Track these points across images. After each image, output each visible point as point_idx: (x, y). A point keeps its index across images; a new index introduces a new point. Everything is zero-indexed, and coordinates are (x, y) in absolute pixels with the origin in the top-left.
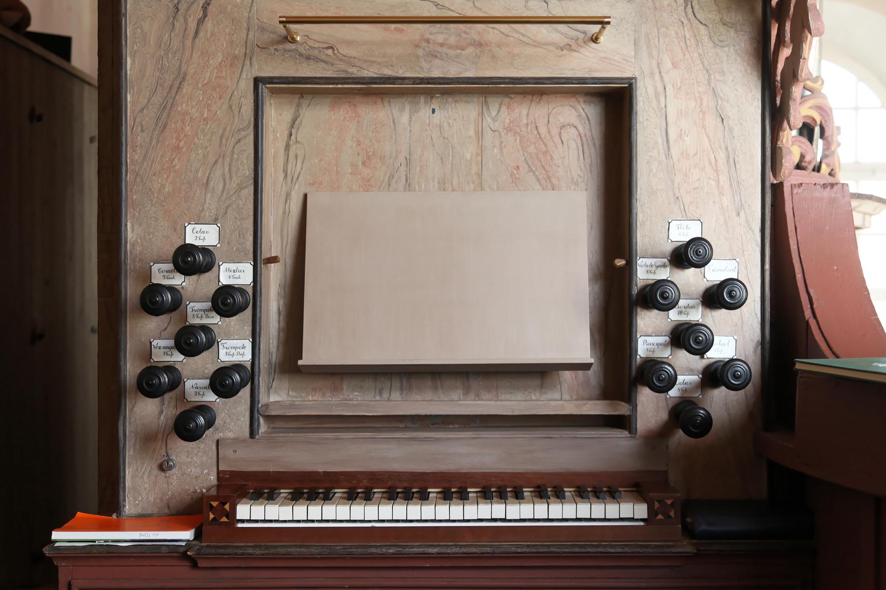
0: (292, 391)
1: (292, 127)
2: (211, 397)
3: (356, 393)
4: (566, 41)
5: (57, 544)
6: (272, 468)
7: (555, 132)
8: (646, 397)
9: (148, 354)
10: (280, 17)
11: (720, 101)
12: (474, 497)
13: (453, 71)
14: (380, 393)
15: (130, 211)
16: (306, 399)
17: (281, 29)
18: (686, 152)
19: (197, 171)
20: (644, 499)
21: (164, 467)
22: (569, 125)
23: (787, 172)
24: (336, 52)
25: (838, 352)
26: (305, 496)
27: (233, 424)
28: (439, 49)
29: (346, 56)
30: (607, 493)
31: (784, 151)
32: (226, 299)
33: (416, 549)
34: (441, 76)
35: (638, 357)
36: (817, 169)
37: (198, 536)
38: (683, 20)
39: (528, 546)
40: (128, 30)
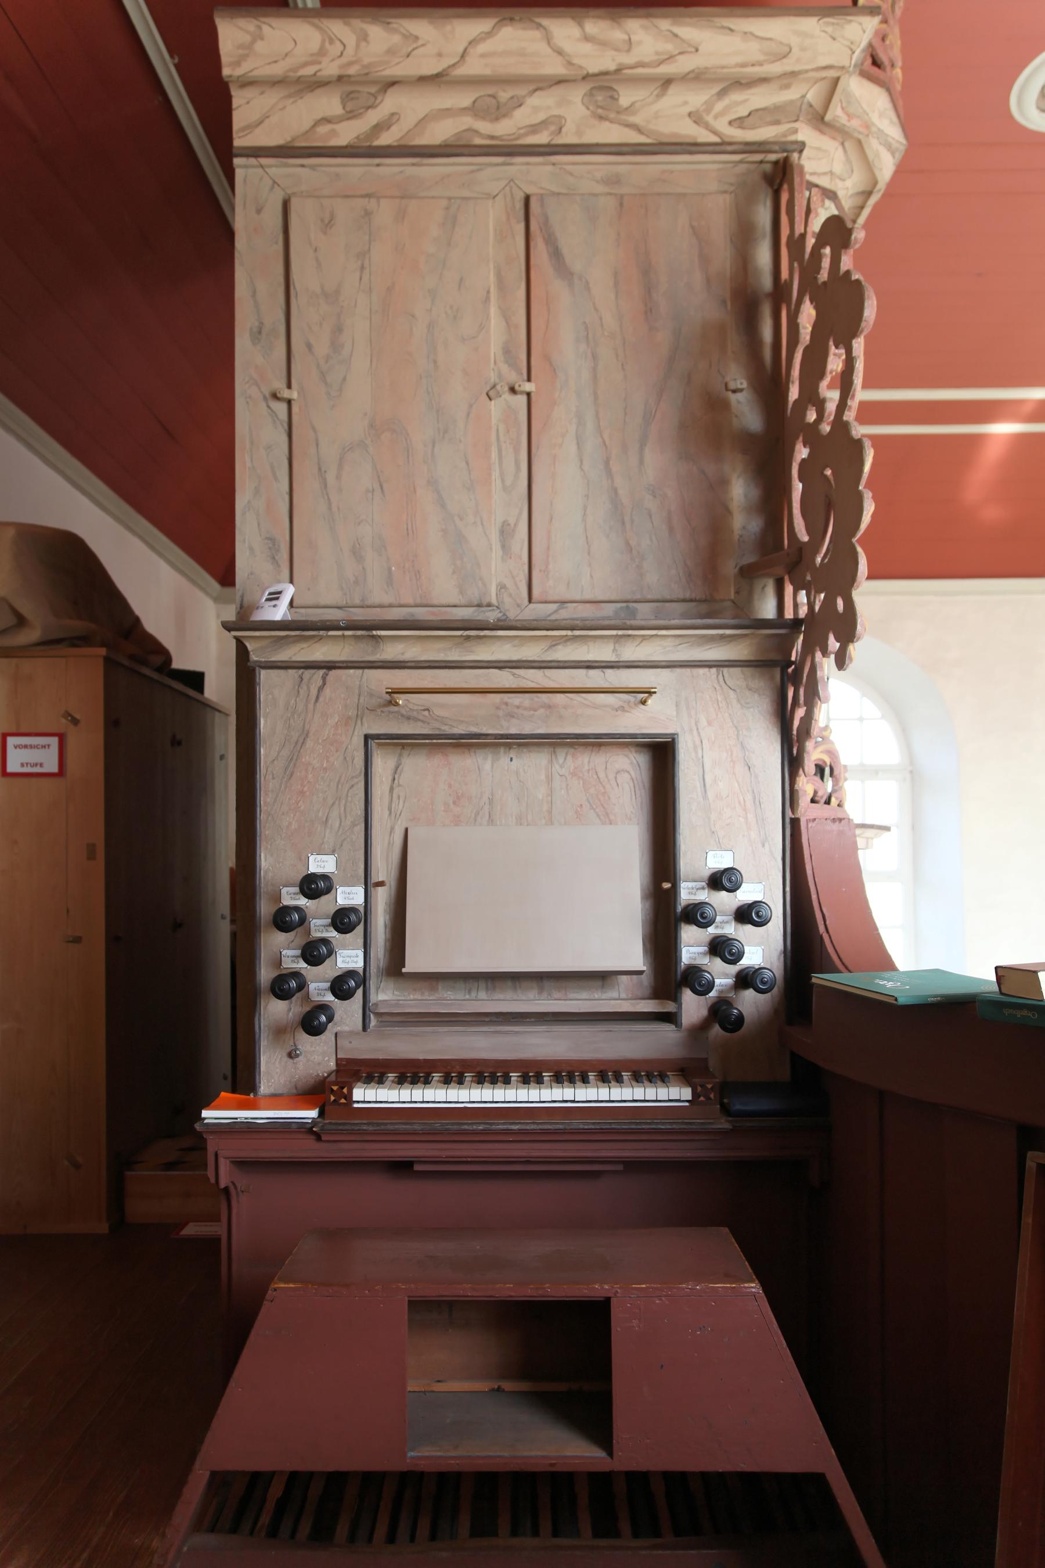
0: (396, 991)
1: (396, 773)
2: (330, 997)
3: (449, 993)
4: (621, 703)
5: (206, 1121)
6: (381, 1056)
7: (611, 776)
8: (688, 997)
9: (279, 963)
10: (387, 688)
11: (747, 753)
12: (548, 1080)
13: (528, 729)
14: (470, 992)
15: (264, 844)
16: (408, 998)
17: (388, 697)
18: (720, 795)
19: (318, 811)
20: (689, 1083)
21: (292, 1055)
22: (623, 771)
23: (803, 810)
24: (431, 713)
25: (850, 967)
26: (409, 1079)
27: (348, 1019)
28: (516, 710)
29: (440, 717)
30: (658, 1077)
31: (800, 793)
32: (343, 919)
33: (501, 1126)
34: (518, 732)
35: (682, 964)
36: (828, 802)
37: (321, 1114)
38: (716, 686)
39: (594, 1124)
40: (261, 696)
